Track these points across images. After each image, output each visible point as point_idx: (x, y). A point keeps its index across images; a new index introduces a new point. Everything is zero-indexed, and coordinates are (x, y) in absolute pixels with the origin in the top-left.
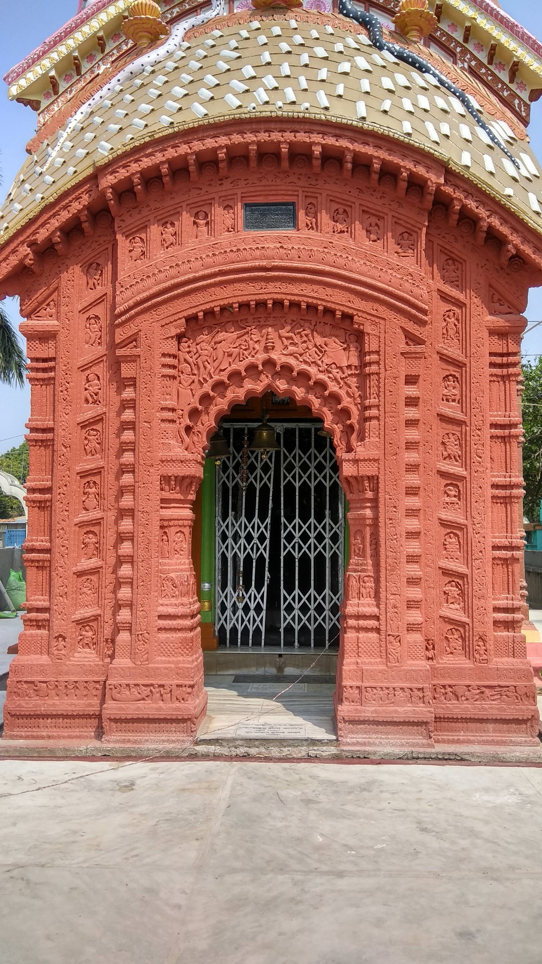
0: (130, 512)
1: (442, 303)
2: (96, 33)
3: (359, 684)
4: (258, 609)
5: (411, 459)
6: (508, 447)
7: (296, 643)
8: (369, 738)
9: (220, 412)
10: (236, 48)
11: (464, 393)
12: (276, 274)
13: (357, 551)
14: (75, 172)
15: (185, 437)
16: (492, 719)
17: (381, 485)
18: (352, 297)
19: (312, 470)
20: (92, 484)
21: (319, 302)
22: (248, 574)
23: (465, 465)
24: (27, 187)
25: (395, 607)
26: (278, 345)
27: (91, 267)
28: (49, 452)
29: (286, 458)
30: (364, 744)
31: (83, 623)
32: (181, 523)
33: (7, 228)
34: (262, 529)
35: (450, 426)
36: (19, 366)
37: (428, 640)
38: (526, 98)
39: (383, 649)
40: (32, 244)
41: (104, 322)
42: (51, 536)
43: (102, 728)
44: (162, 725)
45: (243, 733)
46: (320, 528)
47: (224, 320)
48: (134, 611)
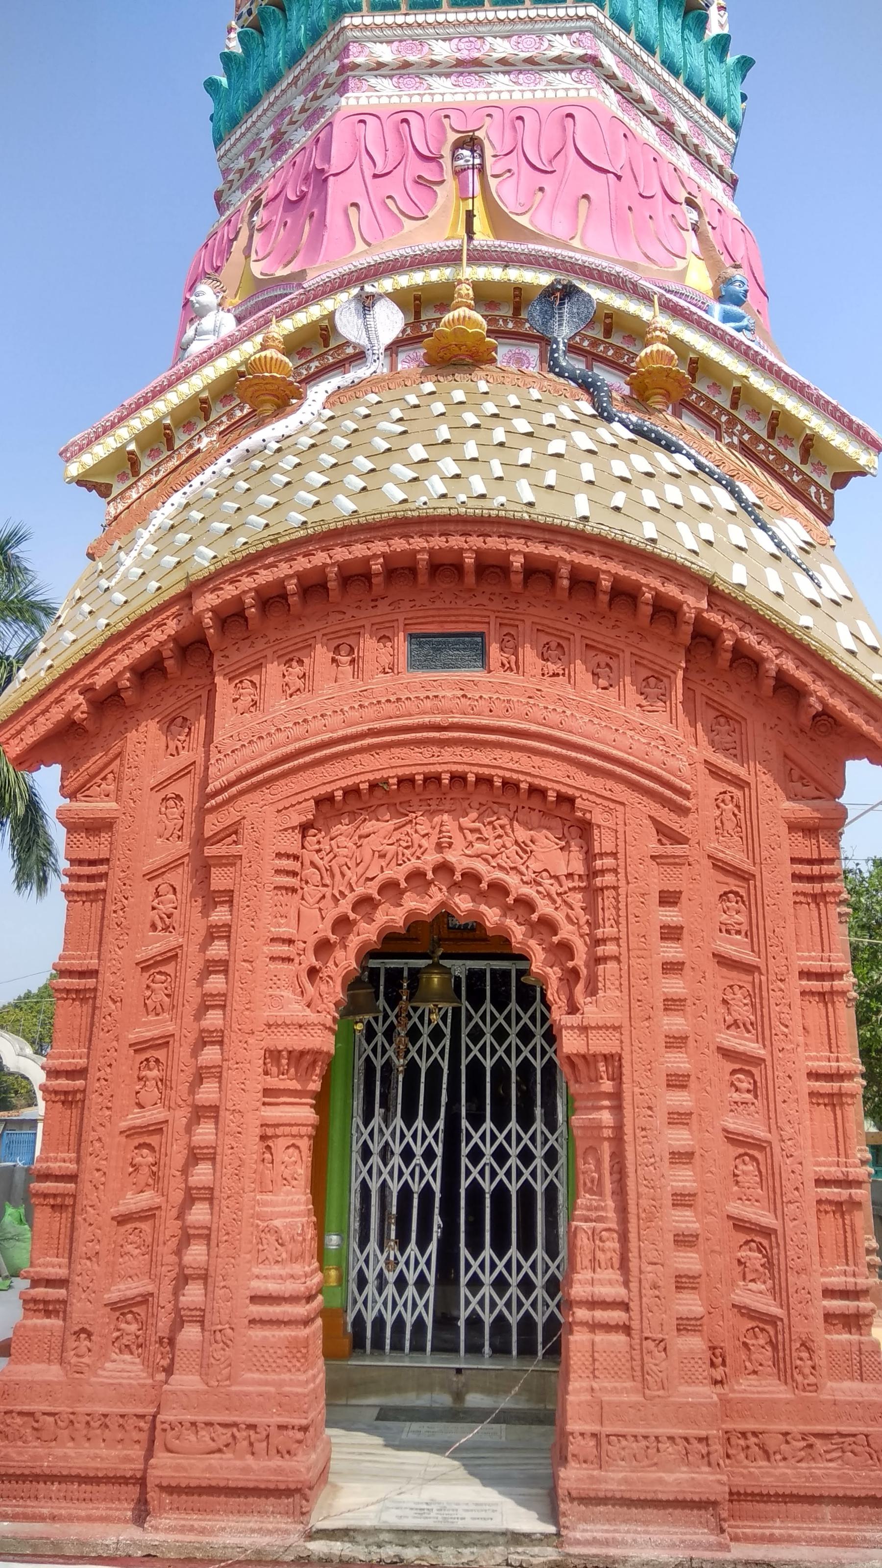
0: (212, 1112)
1: (712, 781)
2: (198, 393)
3: (595, 1428)
4: (421, 1283)
5: (674, 1028)
6: (830, 1009)
7: (487, 1349)
8: (615, 1531)
9: (365, 943)
10: (401, 420)
11: (754, 921)
12: (456, 734)
13: (589, 1184)
14: (159, 588)
15: (308, 985)
16: (829, 1497)
17: (626, 1070)
18: (572, 770)
19: (513, 1039)
20: (152, 1064)
21: (522, 777)
22: (405, 1218)
23: (761, 1039)
24: (86, 607)
25: (655, 1287)
26: (458, 841)
27: (175, 723)
28: (87, 1008)
29: (469, 1018)
30: (606, 1543)
31: (122, 1308)
32: (295, 1130)
33: (51, 667)
34: (430, 1139)
35: (734, 974)
36: (44, 864)
37: (714, 1348)
38: (827, 485)
39: (637, 1364)
40: (87, 690)
41: (188, 805)
42: (78, 1152)
43: (146, 1502)
44: (251, 1500)
45: (392, 1519)
46: (526, 1139)
47: (375, 802)
48: (210, 1288)
